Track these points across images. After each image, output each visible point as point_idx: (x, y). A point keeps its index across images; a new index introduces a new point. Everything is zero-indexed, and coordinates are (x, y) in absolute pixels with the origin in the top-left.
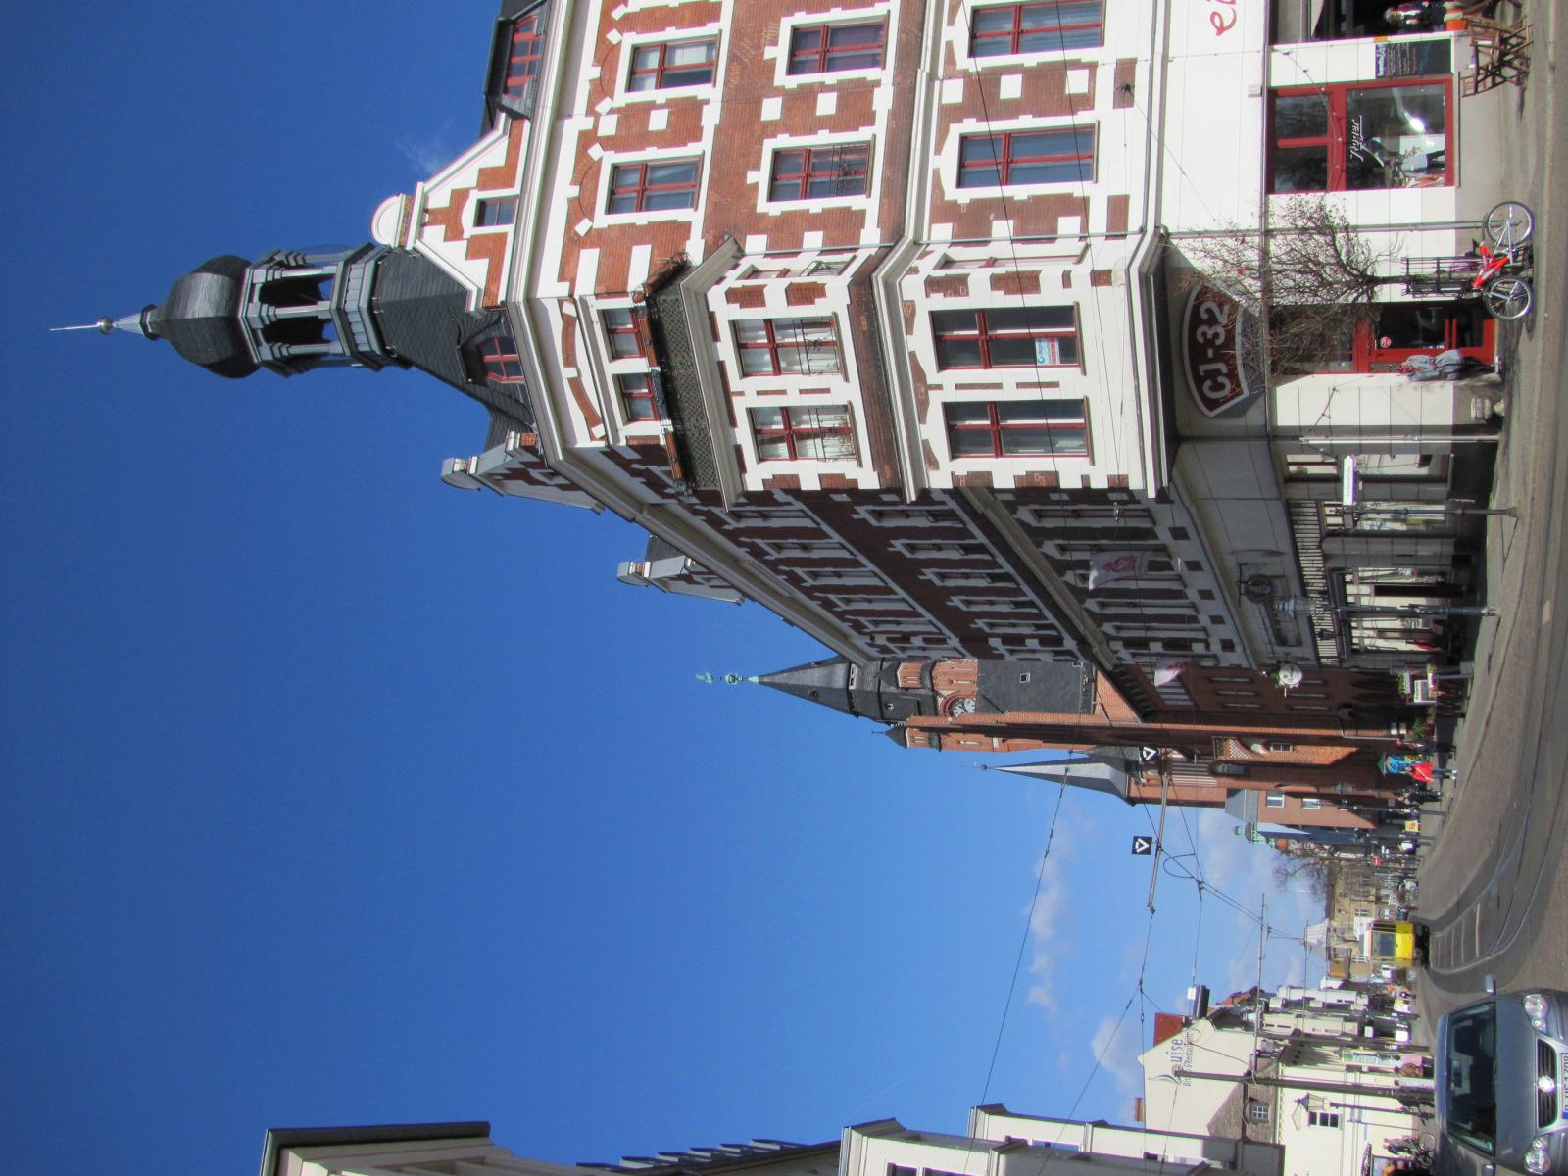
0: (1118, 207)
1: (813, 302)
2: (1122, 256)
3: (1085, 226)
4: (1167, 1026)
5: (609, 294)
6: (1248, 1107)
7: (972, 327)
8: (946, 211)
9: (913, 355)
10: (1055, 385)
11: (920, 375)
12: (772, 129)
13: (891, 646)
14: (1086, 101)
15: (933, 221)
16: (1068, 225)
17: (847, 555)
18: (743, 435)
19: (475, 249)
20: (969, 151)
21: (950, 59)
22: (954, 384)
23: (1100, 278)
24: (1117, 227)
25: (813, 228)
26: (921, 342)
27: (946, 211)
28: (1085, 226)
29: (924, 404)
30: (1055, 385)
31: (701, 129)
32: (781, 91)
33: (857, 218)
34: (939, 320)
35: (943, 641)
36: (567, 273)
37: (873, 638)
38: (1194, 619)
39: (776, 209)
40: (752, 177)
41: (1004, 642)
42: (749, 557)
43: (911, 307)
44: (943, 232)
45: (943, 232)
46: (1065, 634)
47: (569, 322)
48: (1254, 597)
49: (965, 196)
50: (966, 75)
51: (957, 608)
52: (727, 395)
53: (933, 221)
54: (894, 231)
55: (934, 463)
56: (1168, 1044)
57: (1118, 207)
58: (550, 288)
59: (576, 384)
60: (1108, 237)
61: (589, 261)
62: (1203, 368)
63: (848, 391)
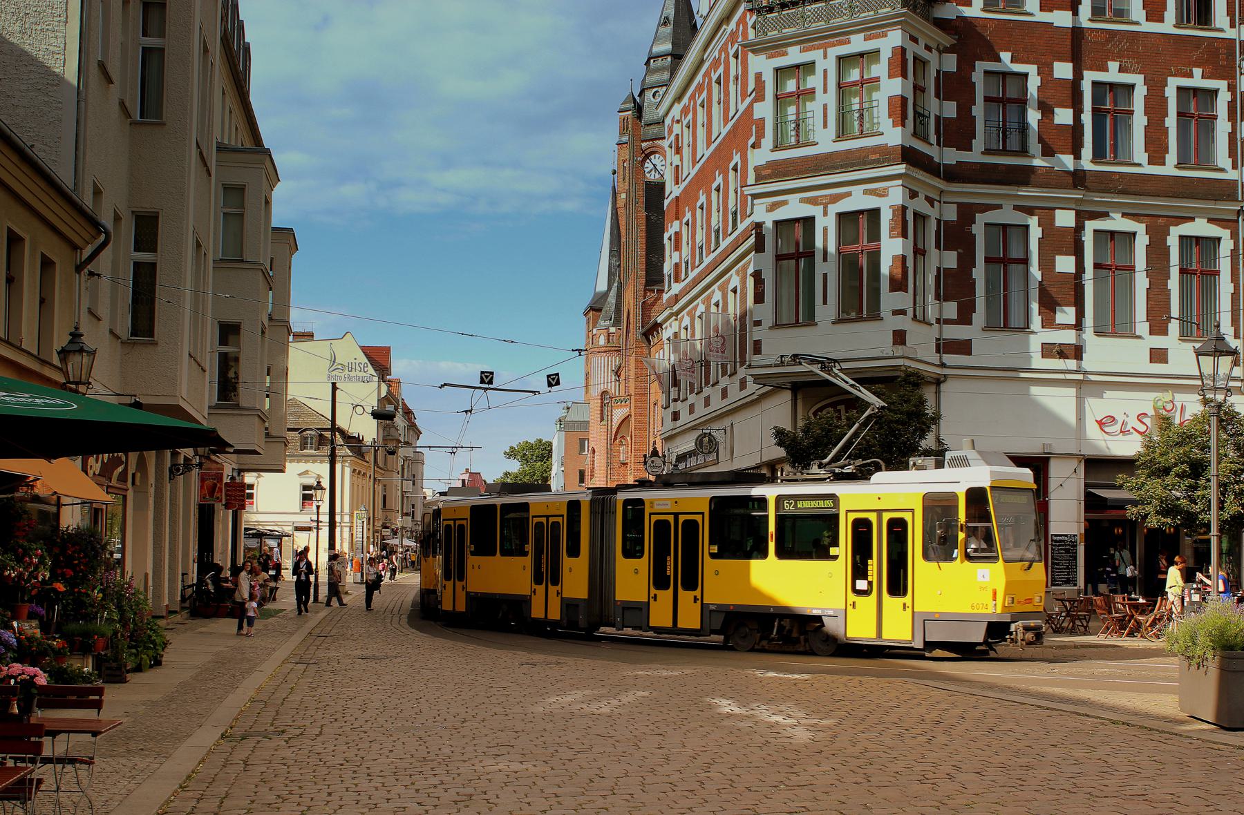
0: (964, 347)
1: (890, 116)
2: (922, 351)
3: (948, 322)
4: (379, 360)
6: (313, 433)
8: (967, 213)
9: (849, 194)
10: (825, 302)
11: (835, 199)
12: (1045, 71)
13: (673, 138)
14: (1049, 323)
15: (959, 205)
16: (951, 309)
17: (731, 115)
18: (794, 55)
20: (1021, 229)
21: (1094, 216)
23: (900, 337)
24: (945, 346)
25: (959, 109)
26: (858, 200)
27: (967, 213)
28: (948, 322)
29: (813, 201)
30: (825, 302)
31: (1051, 11)
32: (1078, 76)
33: (965, 144)
34: (874, 214)
35: (677, 183)
37: (678, 122)
38: (724, 374)
39: (978, 77)
40: (1197, 72)
41: (676, 233)
42: (729, 31)
43: (882, 194)
44: (951, 214)
45: (951, 214)
46: (683, 284)
48: (699, 442)
49: (978, 230)
50: (1079, 228)
51: (698, 199)
53: (959, 205)
54: (954, 174)
55: (772, 208)
56: (365, 360)
57: (964, 347)
60: (938, 339)
62: (842, 407)
63: (825, 141)
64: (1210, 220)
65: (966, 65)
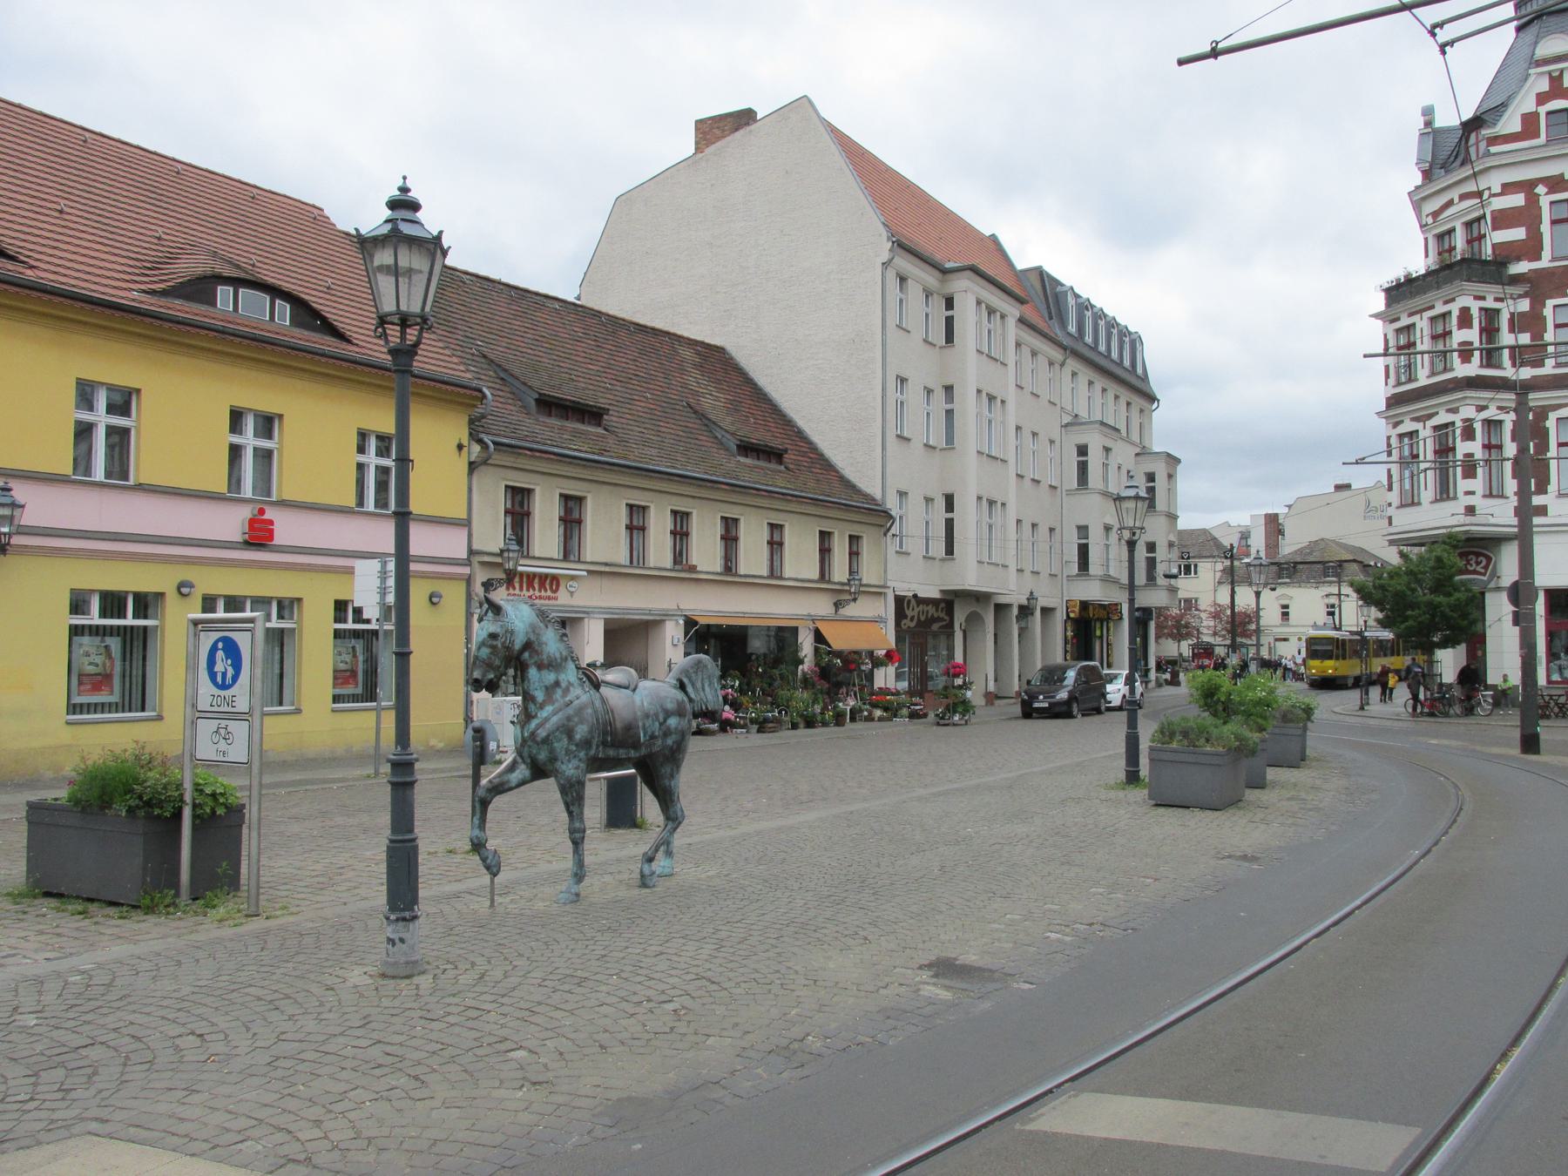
5: (1494, 219)
7: (397, 505)
19: (1530, 121)
22: (1425, 432)
26: (1443, 418)
36: (1508, 188)
39: (1548, 312)
47: (1479, 194)
52: (1420, 312)
58: (1495, 181)
59: (1450, 203)
61: (1518, 200)
63: (1423, 379)
64: (1413, 419)
65: (1538, 303)
